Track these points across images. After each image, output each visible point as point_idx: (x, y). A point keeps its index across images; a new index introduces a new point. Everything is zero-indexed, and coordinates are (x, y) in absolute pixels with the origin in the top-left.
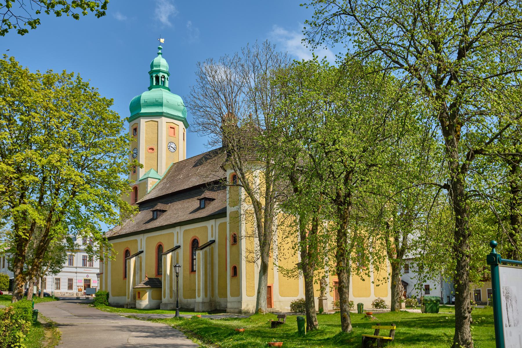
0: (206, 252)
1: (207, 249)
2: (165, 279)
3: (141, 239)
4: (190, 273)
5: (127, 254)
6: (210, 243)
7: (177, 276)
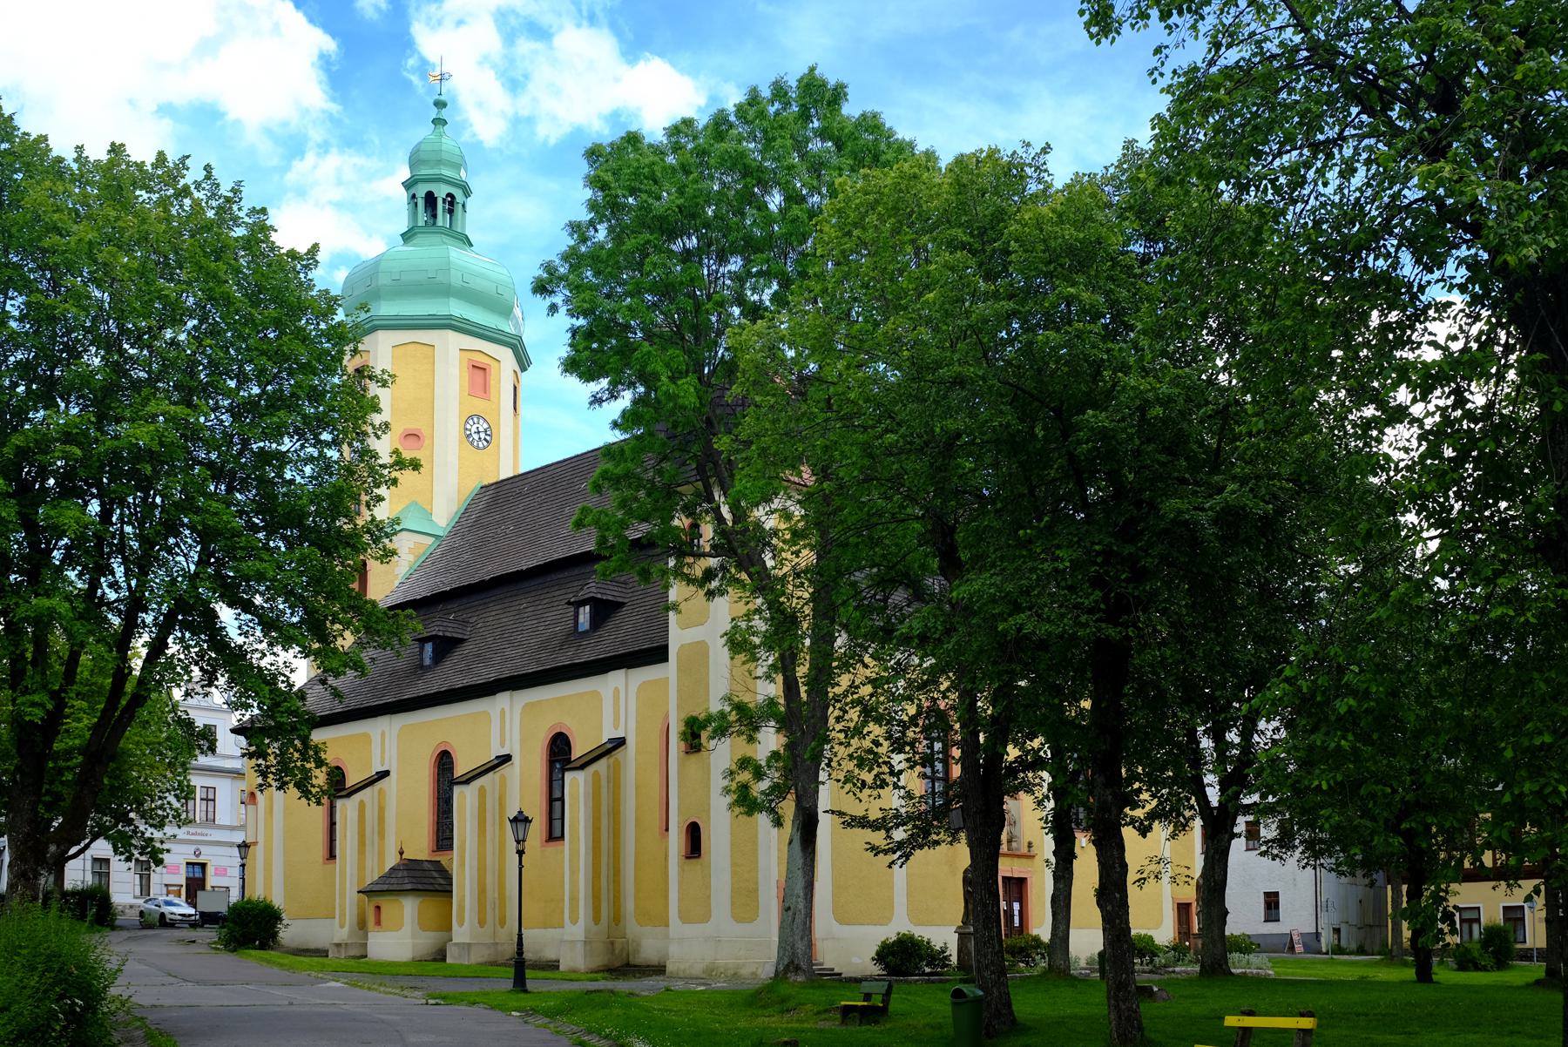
0: (596, 774)
1: (601, 766)
2: (462, 864)
3: (383, 734)
6: (609, 746)
7: (520, 853)
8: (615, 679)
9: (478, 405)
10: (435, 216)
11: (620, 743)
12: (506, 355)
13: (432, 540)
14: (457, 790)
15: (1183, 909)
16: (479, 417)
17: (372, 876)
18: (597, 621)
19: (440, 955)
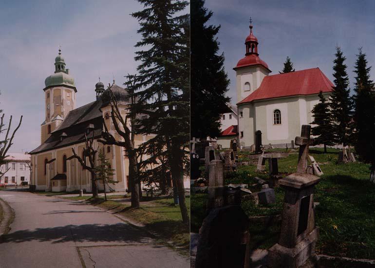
5: (46, 161)
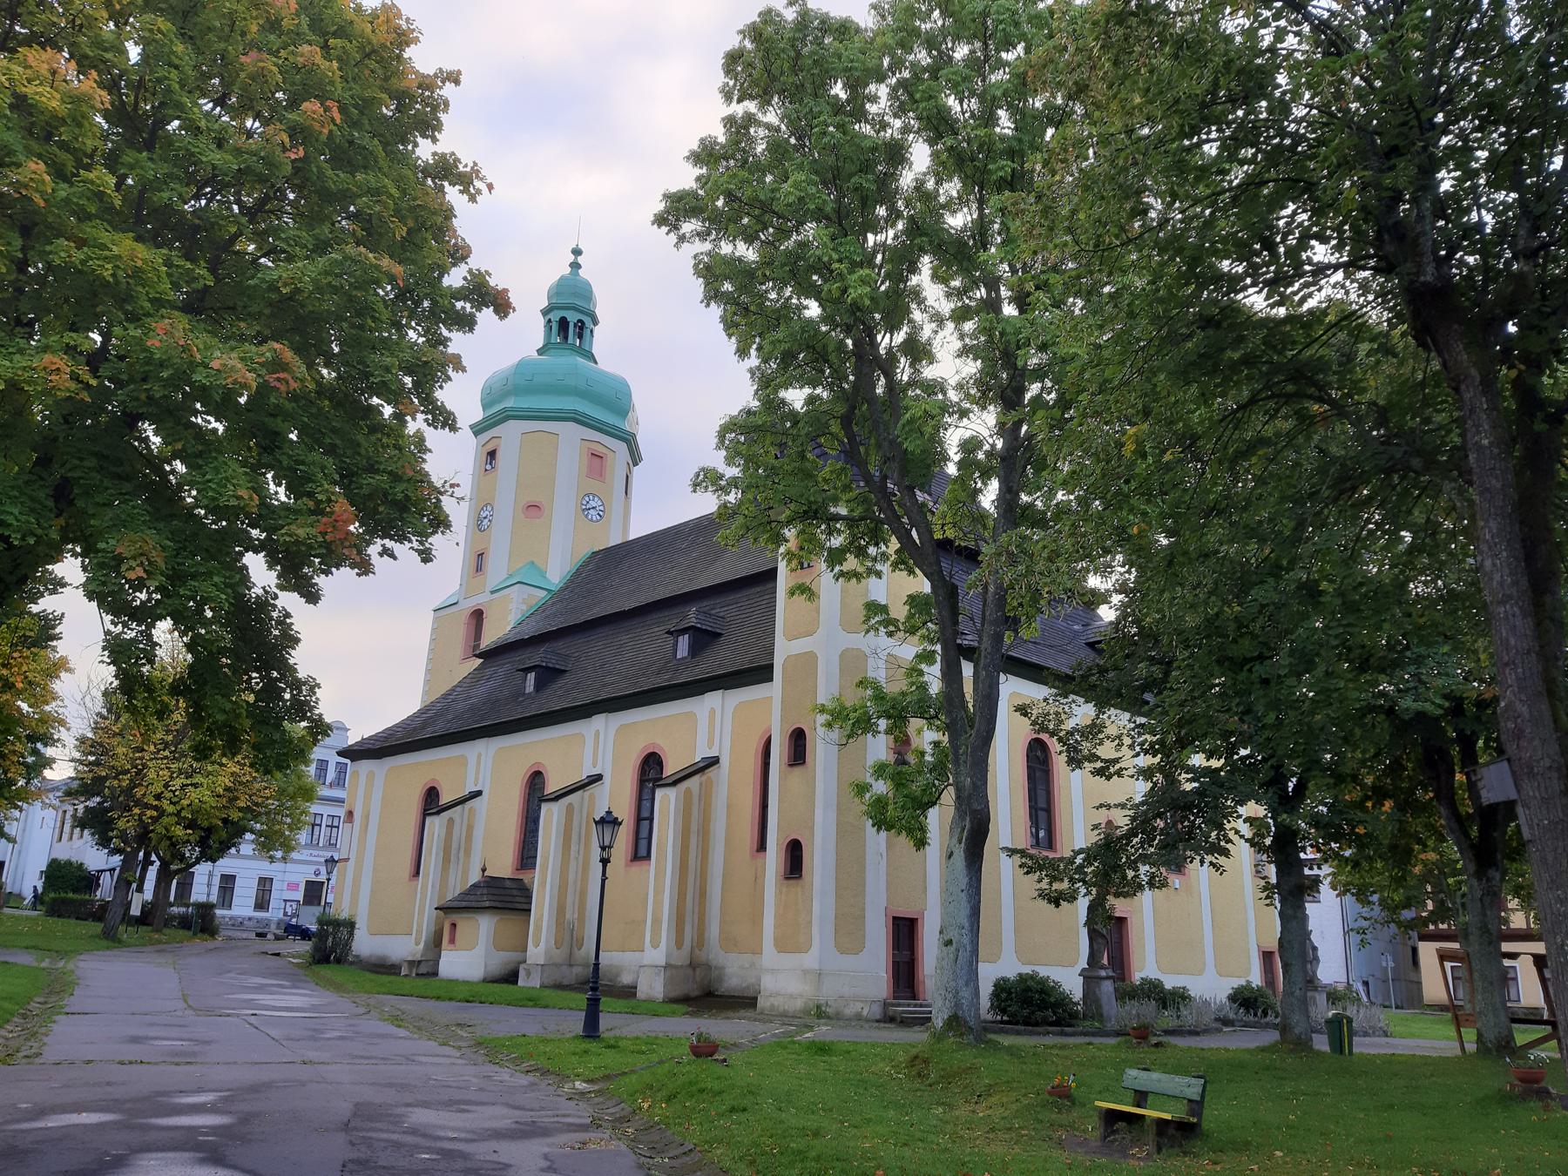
0: (688, 791)
1: (693, 783)
2: (543, 883)
3: (479, 756)
4: (627, 865)
5: (431, 802)
6: (702, 765)
7: (605, 862)
8: (713, 700)
9: (594, 486)
10: (566, 338)
11: (713, 762)
12: (622, 447)
13: (543, 594)
14: (545, 807)
15: (1267, 956)
16: (594, 495)
17: (454, 890)
18: (695, 650)
19: (511, 977)
